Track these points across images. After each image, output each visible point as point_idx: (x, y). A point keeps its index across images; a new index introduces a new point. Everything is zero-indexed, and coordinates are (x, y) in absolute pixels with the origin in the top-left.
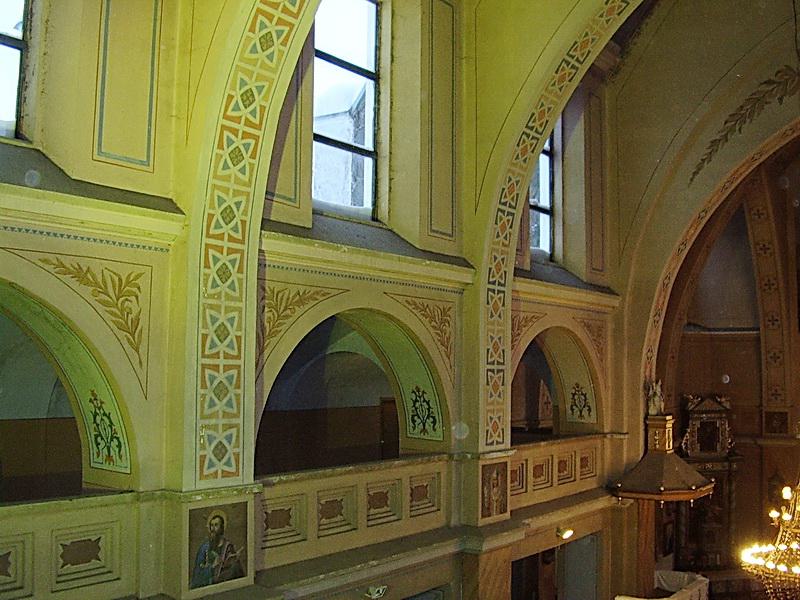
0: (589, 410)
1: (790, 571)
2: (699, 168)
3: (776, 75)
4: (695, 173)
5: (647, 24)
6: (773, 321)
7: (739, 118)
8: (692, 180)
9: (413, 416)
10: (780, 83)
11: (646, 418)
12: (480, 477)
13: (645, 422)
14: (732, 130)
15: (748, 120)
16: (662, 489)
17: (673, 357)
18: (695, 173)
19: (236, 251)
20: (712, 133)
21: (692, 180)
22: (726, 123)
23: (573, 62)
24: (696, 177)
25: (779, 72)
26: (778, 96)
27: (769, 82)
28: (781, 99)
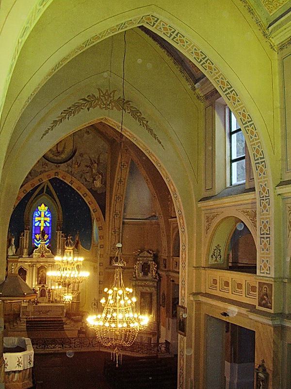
0: (220, 257)
1: (128, 326)
2: (47, 132)
3: (88, 97)
4: (44, 135)
5: (164, 52)
6: (116, 215)
7: (69, 112)
8: (42, 138)
9: (212, 256)
10: (89, 101)
11: (7, 257)
12: (273, 292)
13: (7, 259)
14: (64, 118)
15: (72, 115)
16: (26, 294)
17: (163, 232)
18: (44, 135)
19: (245, 124)
20: (55, 116)
21: (42, 138)
22: (62, 113)
23: (204, 61)
24: (44, 136)
25: (89, 96)
26: (87, 107)
27: (84, 100)
28: (88, 109)
